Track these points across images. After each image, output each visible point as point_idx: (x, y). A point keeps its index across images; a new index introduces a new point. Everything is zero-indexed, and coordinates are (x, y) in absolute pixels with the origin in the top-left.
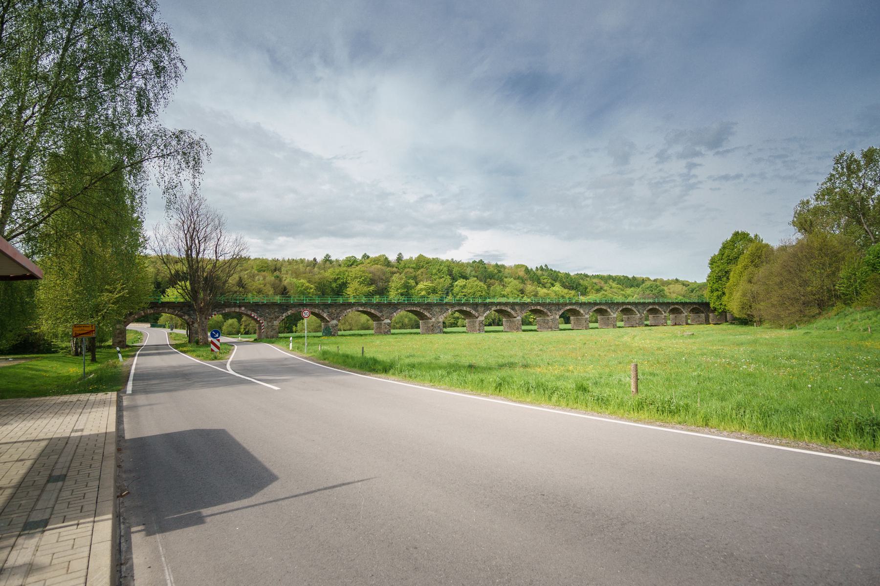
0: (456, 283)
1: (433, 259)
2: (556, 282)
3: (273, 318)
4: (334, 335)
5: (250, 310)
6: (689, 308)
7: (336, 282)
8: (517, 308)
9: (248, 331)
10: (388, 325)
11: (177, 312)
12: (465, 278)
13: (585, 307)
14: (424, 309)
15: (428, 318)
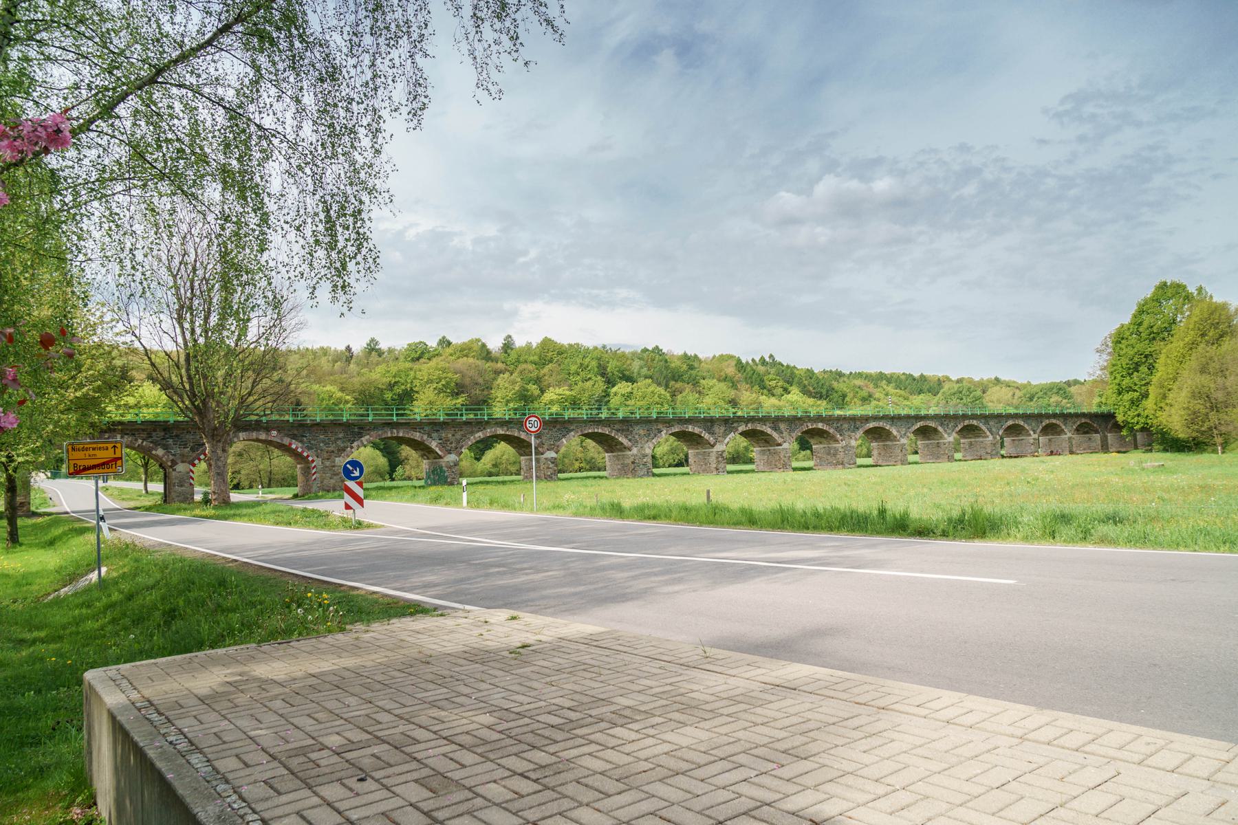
0: (614, 389)
1: (570, 345)
2: (791, 385)
3: (333, 452)
4: (451, 484)
5: (288, 436)
6: (1074, 423)
7: (392, 390)
8: (782, 426)
9: (238, 484)
10: (553, 463)
11: (140, 441)
12: (630, 379)
13: (899, 423)
14: (618, 431)
15: (625, 448)
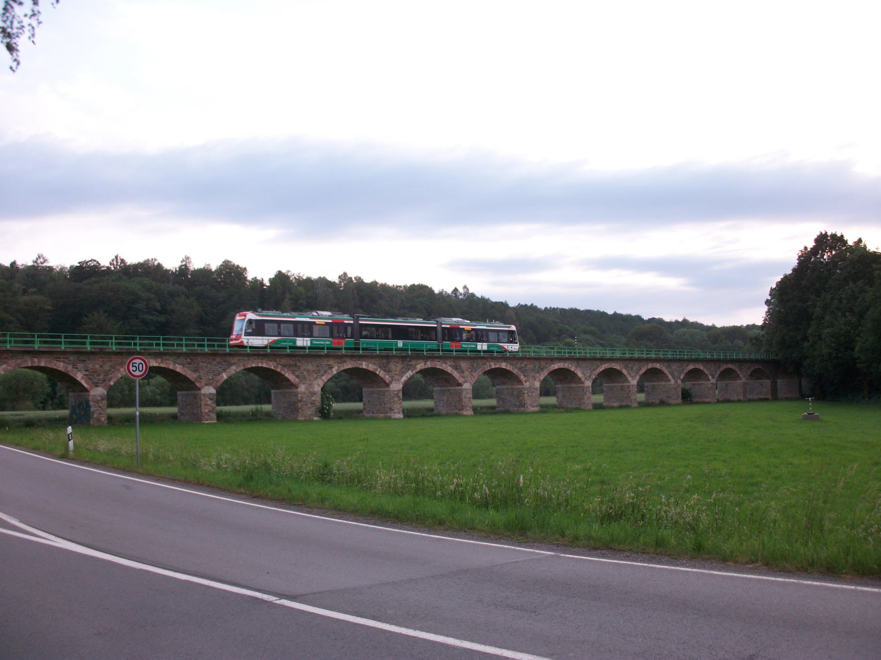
14: (284, 366)
